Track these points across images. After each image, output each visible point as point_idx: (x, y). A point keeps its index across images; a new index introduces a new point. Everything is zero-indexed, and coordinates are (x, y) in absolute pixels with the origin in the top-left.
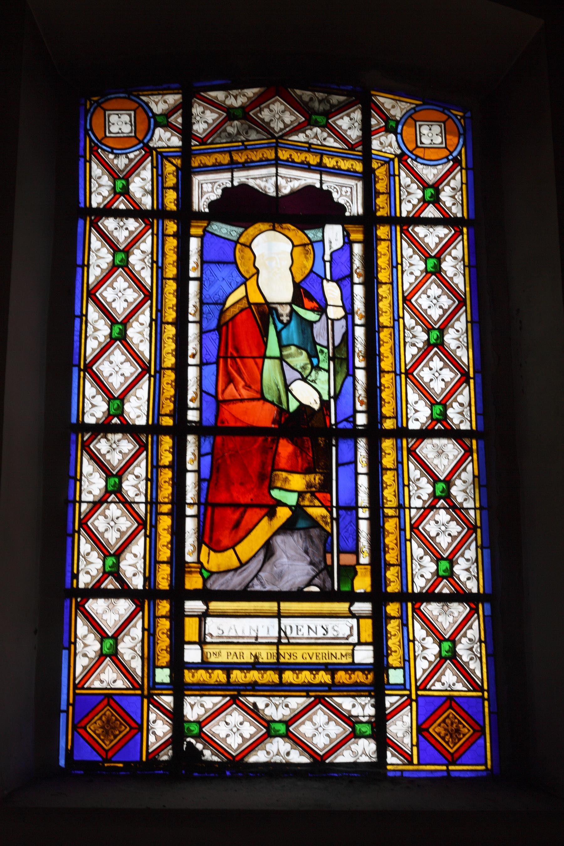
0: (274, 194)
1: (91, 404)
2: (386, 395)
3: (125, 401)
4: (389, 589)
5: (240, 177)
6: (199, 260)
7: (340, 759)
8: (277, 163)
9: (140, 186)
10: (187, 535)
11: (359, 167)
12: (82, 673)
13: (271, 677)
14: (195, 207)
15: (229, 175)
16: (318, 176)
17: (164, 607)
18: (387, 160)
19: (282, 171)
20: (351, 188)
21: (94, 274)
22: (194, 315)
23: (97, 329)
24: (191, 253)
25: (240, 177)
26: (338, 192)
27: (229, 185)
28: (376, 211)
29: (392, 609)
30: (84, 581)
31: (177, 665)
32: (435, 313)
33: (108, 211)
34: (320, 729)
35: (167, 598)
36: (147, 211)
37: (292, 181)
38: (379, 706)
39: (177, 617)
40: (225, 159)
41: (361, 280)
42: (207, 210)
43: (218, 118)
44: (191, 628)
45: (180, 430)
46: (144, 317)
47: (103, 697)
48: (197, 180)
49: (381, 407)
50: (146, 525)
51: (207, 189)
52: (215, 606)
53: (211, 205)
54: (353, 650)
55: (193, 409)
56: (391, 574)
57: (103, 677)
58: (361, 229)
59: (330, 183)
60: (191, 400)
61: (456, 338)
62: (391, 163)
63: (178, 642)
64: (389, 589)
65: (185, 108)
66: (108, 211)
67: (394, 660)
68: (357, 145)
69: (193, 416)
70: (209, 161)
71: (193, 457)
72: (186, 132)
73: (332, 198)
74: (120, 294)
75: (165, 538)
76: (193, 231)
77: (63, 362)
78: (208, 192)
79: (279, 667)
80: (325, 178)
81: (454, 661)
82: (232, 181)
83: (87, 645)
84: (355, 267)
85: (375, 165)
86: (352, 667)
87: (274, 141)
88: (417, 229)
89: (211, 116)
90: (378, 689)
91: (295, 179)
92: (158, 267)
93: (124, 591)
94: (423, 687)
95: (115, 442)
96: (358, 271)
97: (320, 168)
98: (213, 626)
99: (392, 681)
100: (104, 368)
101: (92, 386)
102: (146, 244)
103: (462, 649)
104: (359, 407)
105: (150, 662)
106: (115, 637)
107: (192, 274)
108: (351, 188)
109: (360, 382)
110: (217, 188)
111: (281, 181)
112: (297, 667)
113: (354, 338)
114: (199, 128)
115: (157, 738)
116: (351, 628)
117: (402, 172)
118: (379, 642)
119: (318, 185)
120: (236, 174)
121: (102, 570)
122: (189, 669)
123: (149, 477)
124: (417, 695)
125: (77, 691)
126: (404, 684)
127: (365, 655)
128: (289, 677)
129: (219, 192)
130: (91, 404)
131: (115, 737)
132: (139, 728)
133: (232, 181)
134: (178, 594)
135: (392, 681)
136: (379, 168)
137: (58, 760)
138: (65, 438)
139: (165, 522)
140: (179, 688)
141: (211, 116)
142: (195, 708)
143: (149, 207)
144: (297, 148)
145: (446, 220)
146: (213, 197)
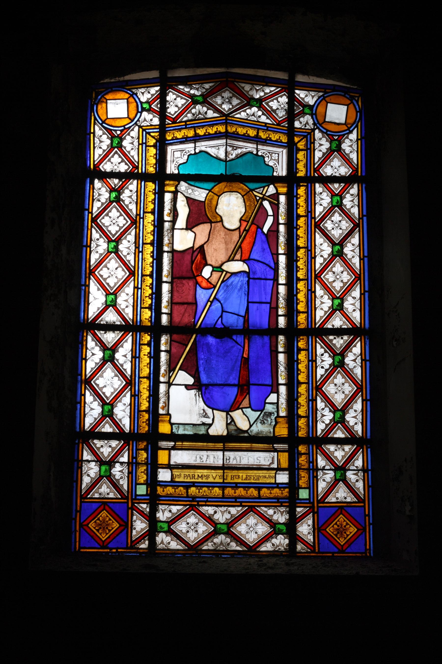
3: (119, 243)
6: (168, 369)
10: (165, 204)
11: (284, 139)
13: (217, 491)
14: (168, 172)
16: (255, 146)
18: (306, 134)
19: (229, 141)
20: (278, 154)
21: (96, 206)
22: (166, 308)
24: (164, 265)
26: (268, 157)
28: (297, 173)
31: (153, 482)
34: (252, 529)
38: (292, 513)
40: (191, 133)
43: (185, 103)
46: (131, 237)
48: (170, 149)
54: (276, 474)
55: (166, 282)
56: (302, 422)
61: (352, 250)
62: (309, 136)
63: (153, 466)
65: (162, 97)
67: (302, 482)
68: (283, 121)
69: (164, 319)
70: (179, 135)
72: (162, 113)
75: (145, 394)
76: (167, 188)
78: (178, 158)
80: (260, 147)
81: (342, 258)
82: (195, 149)
83: (91, 470)
85: (296, 139)
87: (224, 118)
88: (329, 446)
89: (181, 102)
90: (291, 501)
94: (322, 500)
95: (112, 275)
97: (257, 140)
99: (301, 497)
101: (90, 424)
103: (350, 475)
105: (133, 482)
106: (115, 294)
107: (165, 279)
108: (278, 154)
110: (184, 155)
111: (229, 149)
113: (278, 293)
114: (172, 110)
116: (273, 458)
118: (293, 469)
120: (198, 144)
121: (107, 249)
124: (318, 507)
126: (309, 499)
127: (283, 478)
128: (229, 492)
131: (110, 519)
132: (126, 525)
133: (195, 149)
135: (301, 497)
136: (299, 142)
139: (145, 384)
140: (154, 500)
141: (181, 102)
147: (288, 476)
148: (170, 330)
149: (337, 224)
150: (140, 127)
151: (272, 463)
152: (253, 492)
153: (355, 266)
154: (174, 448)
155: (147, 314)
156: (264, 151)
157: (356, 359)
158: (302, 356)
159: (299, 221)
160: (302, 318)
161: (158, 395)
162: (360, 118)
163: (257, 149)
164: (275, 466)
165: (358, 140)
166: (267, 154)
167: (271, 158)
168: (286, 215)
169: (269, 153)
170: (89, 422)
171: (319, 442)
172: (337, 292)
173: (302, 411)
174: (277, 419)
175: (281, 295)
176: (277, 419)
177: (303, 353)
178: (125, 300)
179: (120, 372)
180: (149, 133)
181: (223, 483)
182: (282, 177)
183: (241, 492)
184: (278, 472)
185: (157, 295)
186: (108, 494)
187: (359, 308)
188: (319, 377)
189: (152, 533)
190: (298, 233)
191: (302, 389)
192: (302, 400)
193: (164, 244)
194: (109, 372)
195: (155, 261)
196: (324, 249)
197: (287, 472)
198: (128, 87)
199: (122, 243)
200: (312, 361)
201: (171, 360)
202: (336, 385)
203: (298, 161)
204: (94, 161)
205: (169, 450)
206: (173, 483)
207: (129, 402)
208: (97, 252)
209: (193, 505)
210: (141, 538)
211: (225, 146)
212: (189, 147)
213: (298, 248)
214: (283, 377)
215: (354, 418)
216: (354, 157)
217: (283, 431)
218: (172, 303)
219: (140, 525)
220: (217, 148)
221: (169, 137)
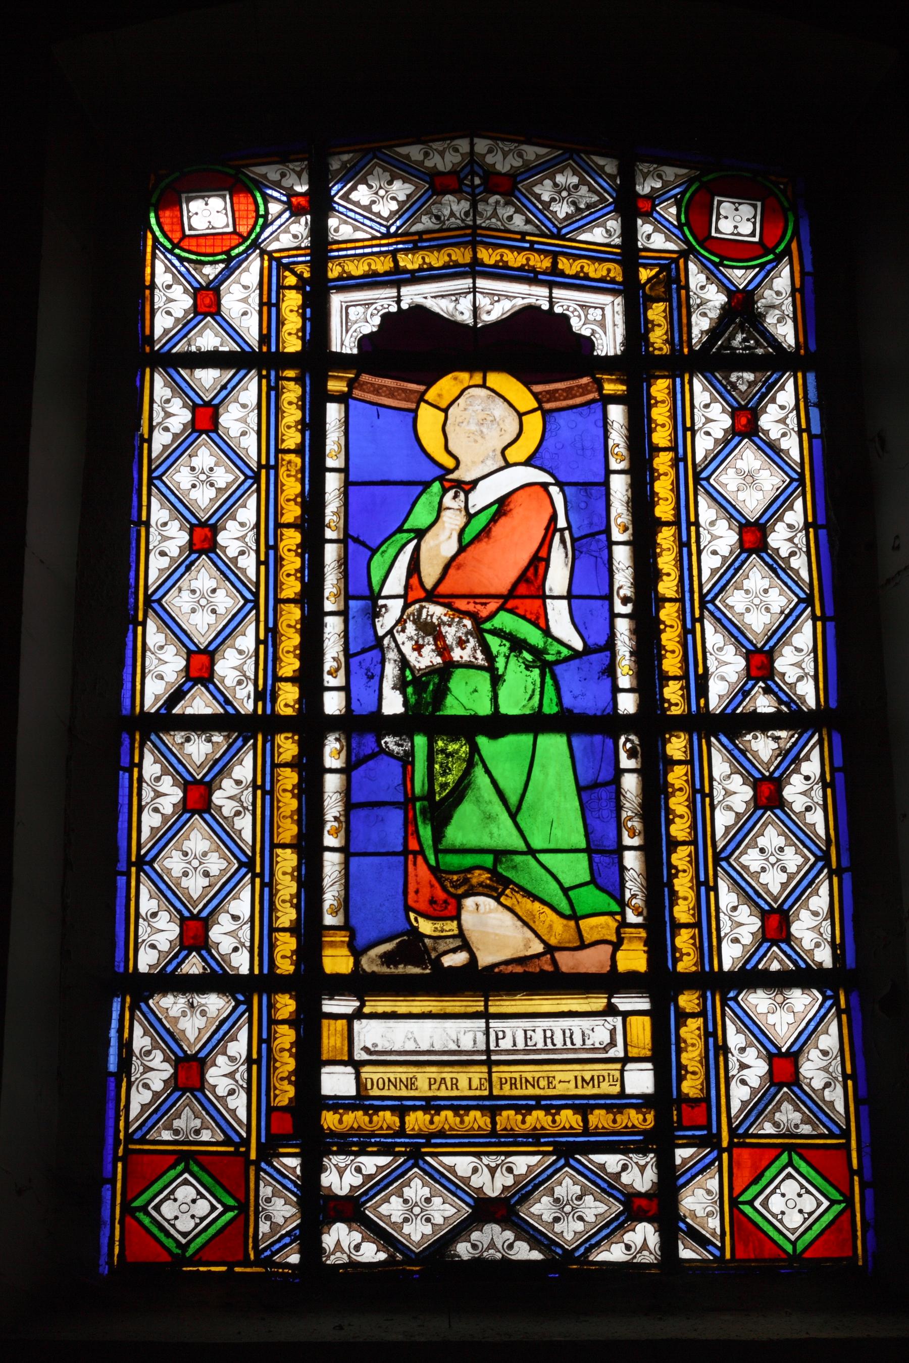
0: (470, 321)
1: (154, 790)
2: (670, 638)
4: (681, 967)
5: (412, 295)
7: (602, 1256)
8: (475, 270)
9: (240, 300)
10: (327, 643)
11: (616, 272)
12: (158, 579)
13: (477, 1120)
14: (335, 347)
15: (393, 292)
17: (286, 1005)
19: (481, 283)
20: (603, 309)
23: (166, 537)
25: (412, 295)
26: (579, 316)
27: (393, 309)
29: (688, 1001)
30: (146, 960)
31: (310, 1097)
32: (773, 881)
33: (168, 981)
35: (293, 992)
36: (239, 977)
37: (499, 300)
39: (309, 1023)
41: (628, 609)
42: (355, 351)
44: (331, 1038)
45: (311, 725)
47: (175, 1157)
48: (337, 300)
49: (679, 1051)
50: (253, 866)
51: (354, 320)
52: (375, 1005)
53: (364, 341)
54: (622, 1071)
57: (176, 1123)
58: (619, 353)
59: (567, 300)
60: (329, 673)
62: (673, 266)
63: (310, 1061)
64: (681, 967)
66: (168, 981)
69: (333, 704)
71: (335, 664)
73: (570, 327)
74: (203, 602)
75: (287, 887)
77: (112, 604)
79: (492, 1106)
80: (558, 293)
82: (398, 302)
84: (613, 514)
86: (619, 1102)
91: (522, 889)
92: (263, 885)
93: (217, 980)
96: (617, 450)
98: (371, 1034)
100: (179, 603)
102: (244, 770)
104: (614, 465)
107: (330, 463)
109: (628, 795)
110: (372, 315)
111: (483, 301)
112: (524, 1106)
115: (275, 1227)
116: (613, 1032)
117: (720, 882)
118: (662, 1055)
119: (545, 306)
120: (404, 290)
122: (329, 1108)
123: (255, 1056)
125: (131, 1147)
128: (508, 1119)
129: (377, 320)
130: (154, 790)
132: (245, 1209)
134: (311, 984)
137: (106, 1061)
138: (114, 730)
139: (287, 860)
142: (340, 1177)
143: (244, 970)
144: (534, 1140)
145: (791, 718)
146: (367, 329)
147: (651, 1074)
148: (348, 723)
149: (751, 469)
150: (263, 252)
151: (613, 1043)
152: (569, 1118)
153: (833, 1108)
154: (359, 1014)
155: (289, 694)
156: (566, 303)
157: (786, 417)
158: (677, 776)
159: (674, 857)
160: (672, 691)
161: (323, 493)
162: (796, 233)
163: (551, 297)
164: (618, 1052)
165: (807, 526)
166: (575, 310)
167: (586, 316)
168: (634, 637)
169: (581, 306)
170: (154, 692)
171: (723, 985)
172: (760, 619)
173: (682, 912)
174: (622, 930)
175: (616, 425)
176: (622, 930)
177: (694, 1024)
178: (234, 668)
179: (224, 835)
180: (287, 267)
181: (491, 1097)
182: (616, 356)
183: (538, 1118)
184: (629, 1066)
185: (313, 502)
186: (197, 1132)
187: (821, 802)
188: (720, 831)
189: (308, 1235)
190: (684, 1061)
191: (680, 857)
192: (683, 885)
193: (327, 451)
194: (198, 839)
195: (308, 324)
196: (719, 539)
197: (649, 1066)
198: (235, 184)
199: (220, 788)
200: (702, 795)
201: (351, 904)
202: (762, 851)
203: (673, 871)
204: (127, 1124)
205: (350, 1018)
206: (361, 1101)
207: (254, 520)
208: (166, 429)
209: (413, 1152)
210: (282, 1242)
211: (471, 296)
212: (384, 300)
213: (677, 926)
214: (626, 669)
215: (798, 665)
216: (799, 563)
217: (633, 959)
218: (350, 806)
219: (282, 1211)
220: (454, 298)
221: (334, 272)
